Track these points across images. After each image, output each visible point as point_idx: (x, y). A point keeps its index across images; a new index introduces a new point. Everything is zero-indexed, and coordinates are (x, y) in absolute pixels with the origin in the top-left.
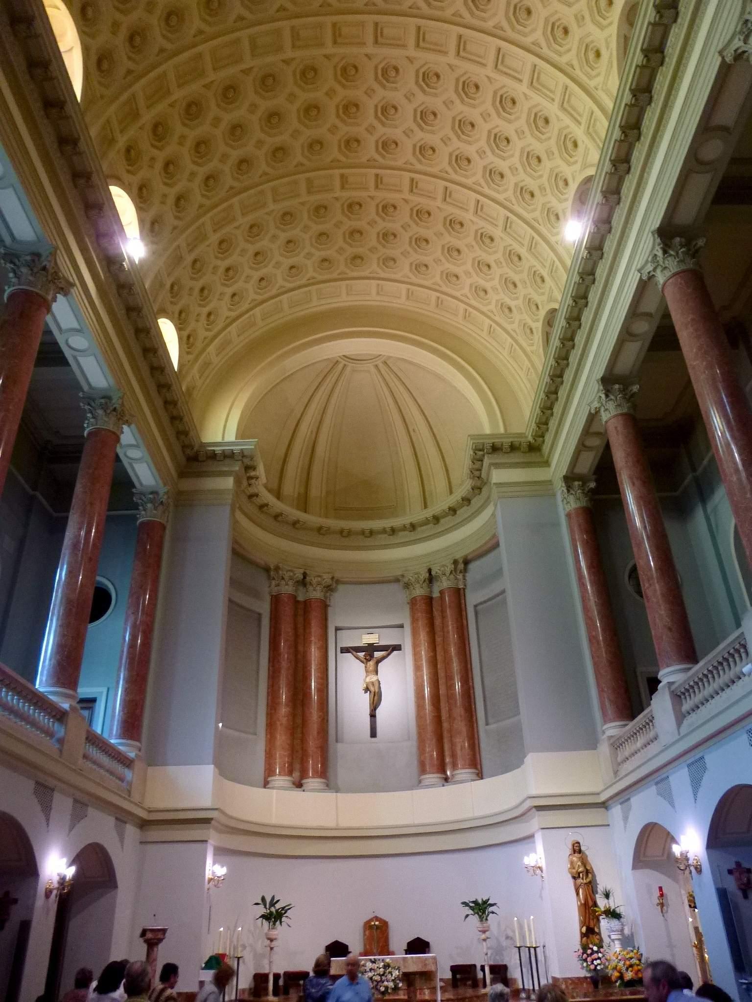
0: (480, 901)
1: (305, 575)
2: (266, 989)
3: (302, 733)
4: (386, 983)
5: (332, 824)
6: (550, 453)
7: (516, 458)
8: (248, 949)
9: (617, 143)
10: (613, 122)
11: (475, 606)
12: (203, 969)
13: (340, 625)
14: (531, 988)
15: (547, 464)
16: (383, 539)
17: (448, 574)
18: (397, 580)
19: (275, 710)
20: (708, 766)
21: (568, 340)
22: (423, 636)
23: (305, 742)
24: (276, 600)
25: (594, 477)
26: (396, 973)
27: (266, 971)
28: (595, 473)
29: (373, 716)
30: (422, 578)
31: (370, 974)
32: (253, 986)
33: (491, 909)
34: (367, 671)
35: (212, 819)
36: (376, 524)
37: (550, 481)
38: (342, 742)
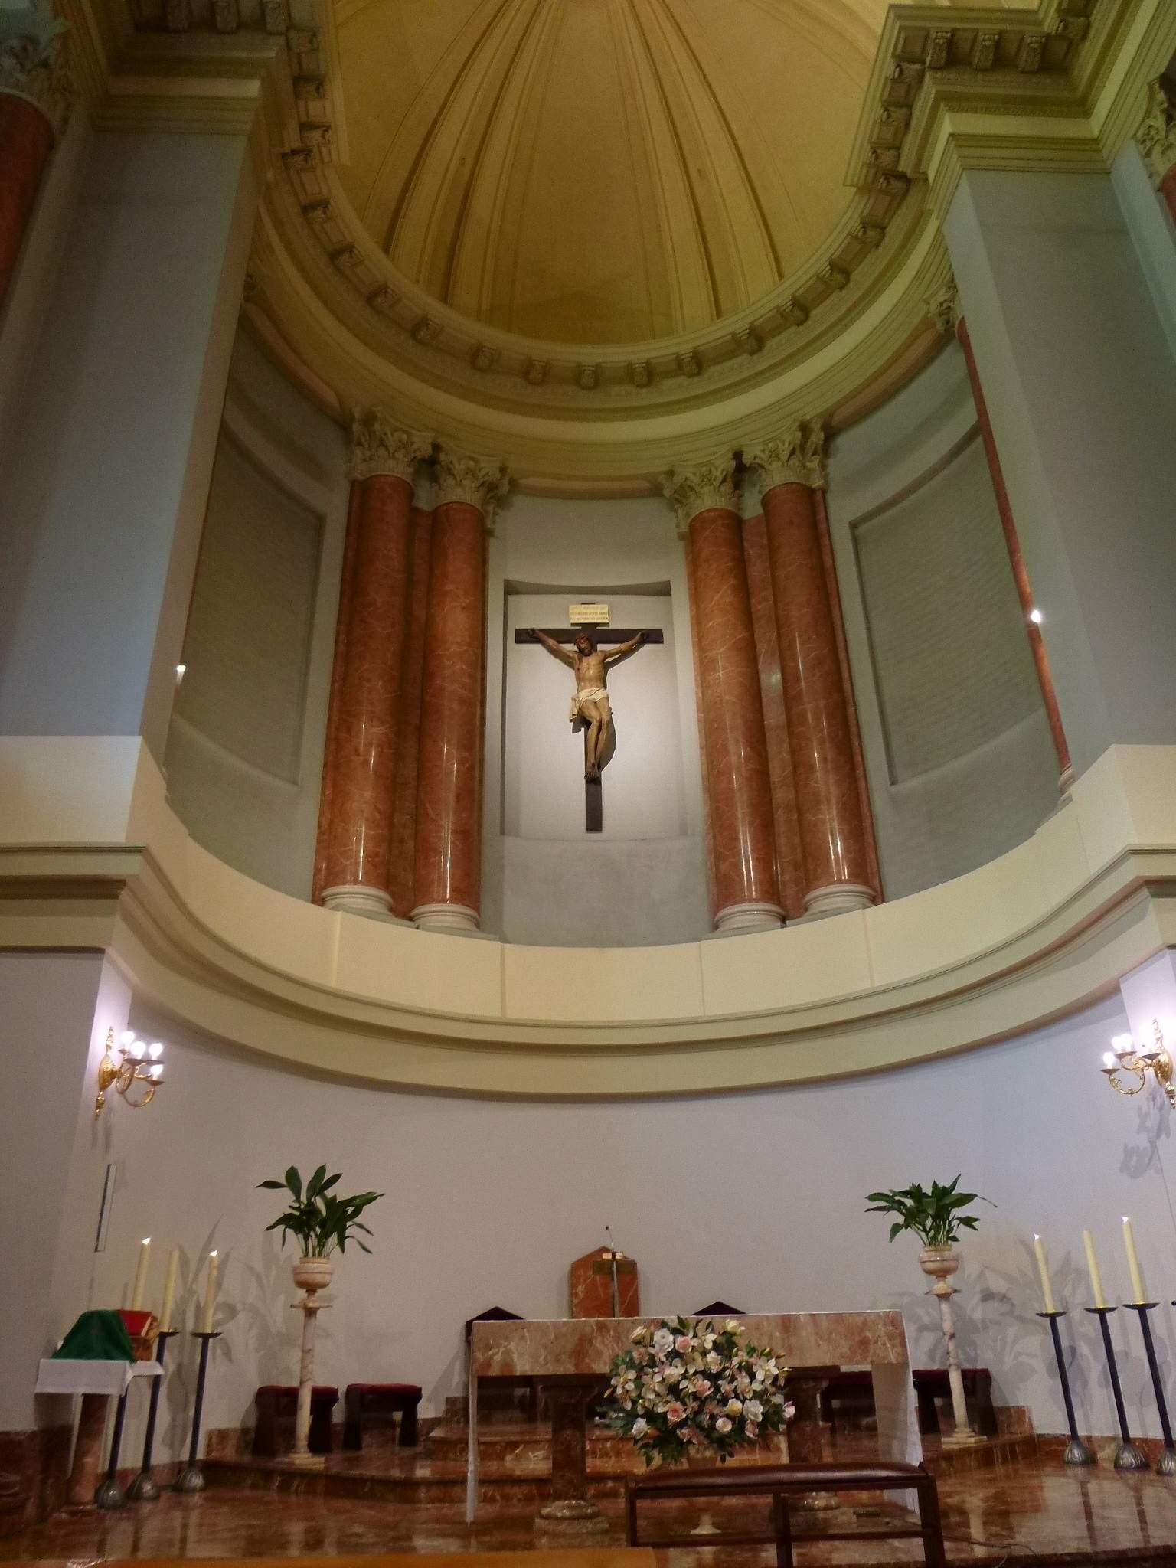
0: (928, 1190)
1: (436, 447)
2: (291, 1432)
3: (417, 798)
4: (735, 1405)
5: (493, 1012)
7: (1003, 85)
8: (241, 1317)
11: (854, 526)
12: (58, 1354)
13: (513, 576)
14: (1157, 1433)
15: (1082, 107)
16: (623, 395)
17: (784, 456)
18: (655, 491)
19: (349, 730)
22: (721, 596)
23: (422, 818)
24: (363, 493)
26: (767, 1369)
27: (295, 1384)
29: (593, 781)
30: (718, 474)
31: (674, 1372)
32: (252, 1423)
33: (957, 1212)
34: (579, 679)
35: (121, 883)
36: (613, 355)
38: (517, 835)
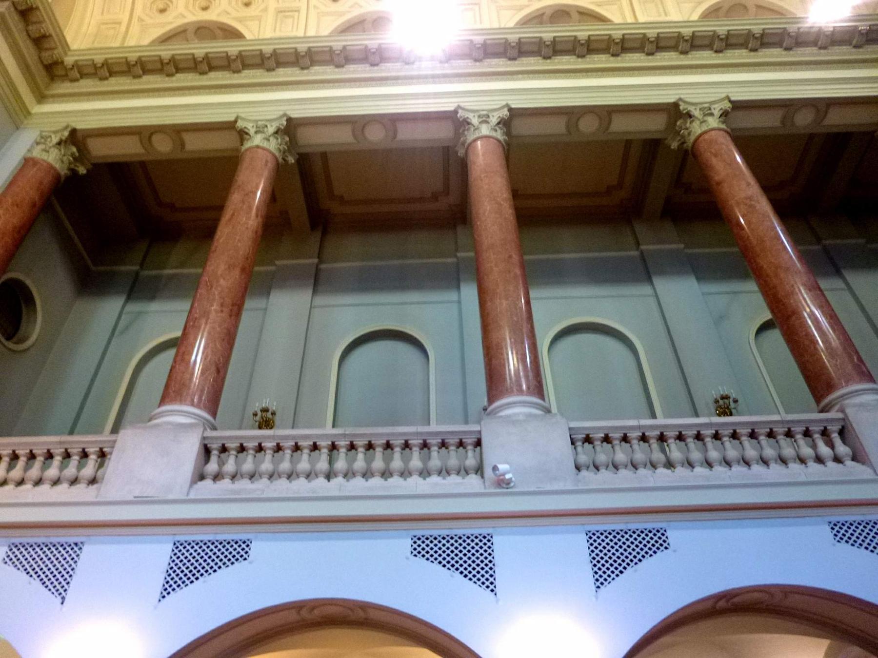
6: (53, 96)
9: (90, 63)
10: (120, 50)
15: (41, 98)
20: (844, 547)
21: (204, 65)
25: (90, 166)
28: (95, 165)
37: (29, 113)
